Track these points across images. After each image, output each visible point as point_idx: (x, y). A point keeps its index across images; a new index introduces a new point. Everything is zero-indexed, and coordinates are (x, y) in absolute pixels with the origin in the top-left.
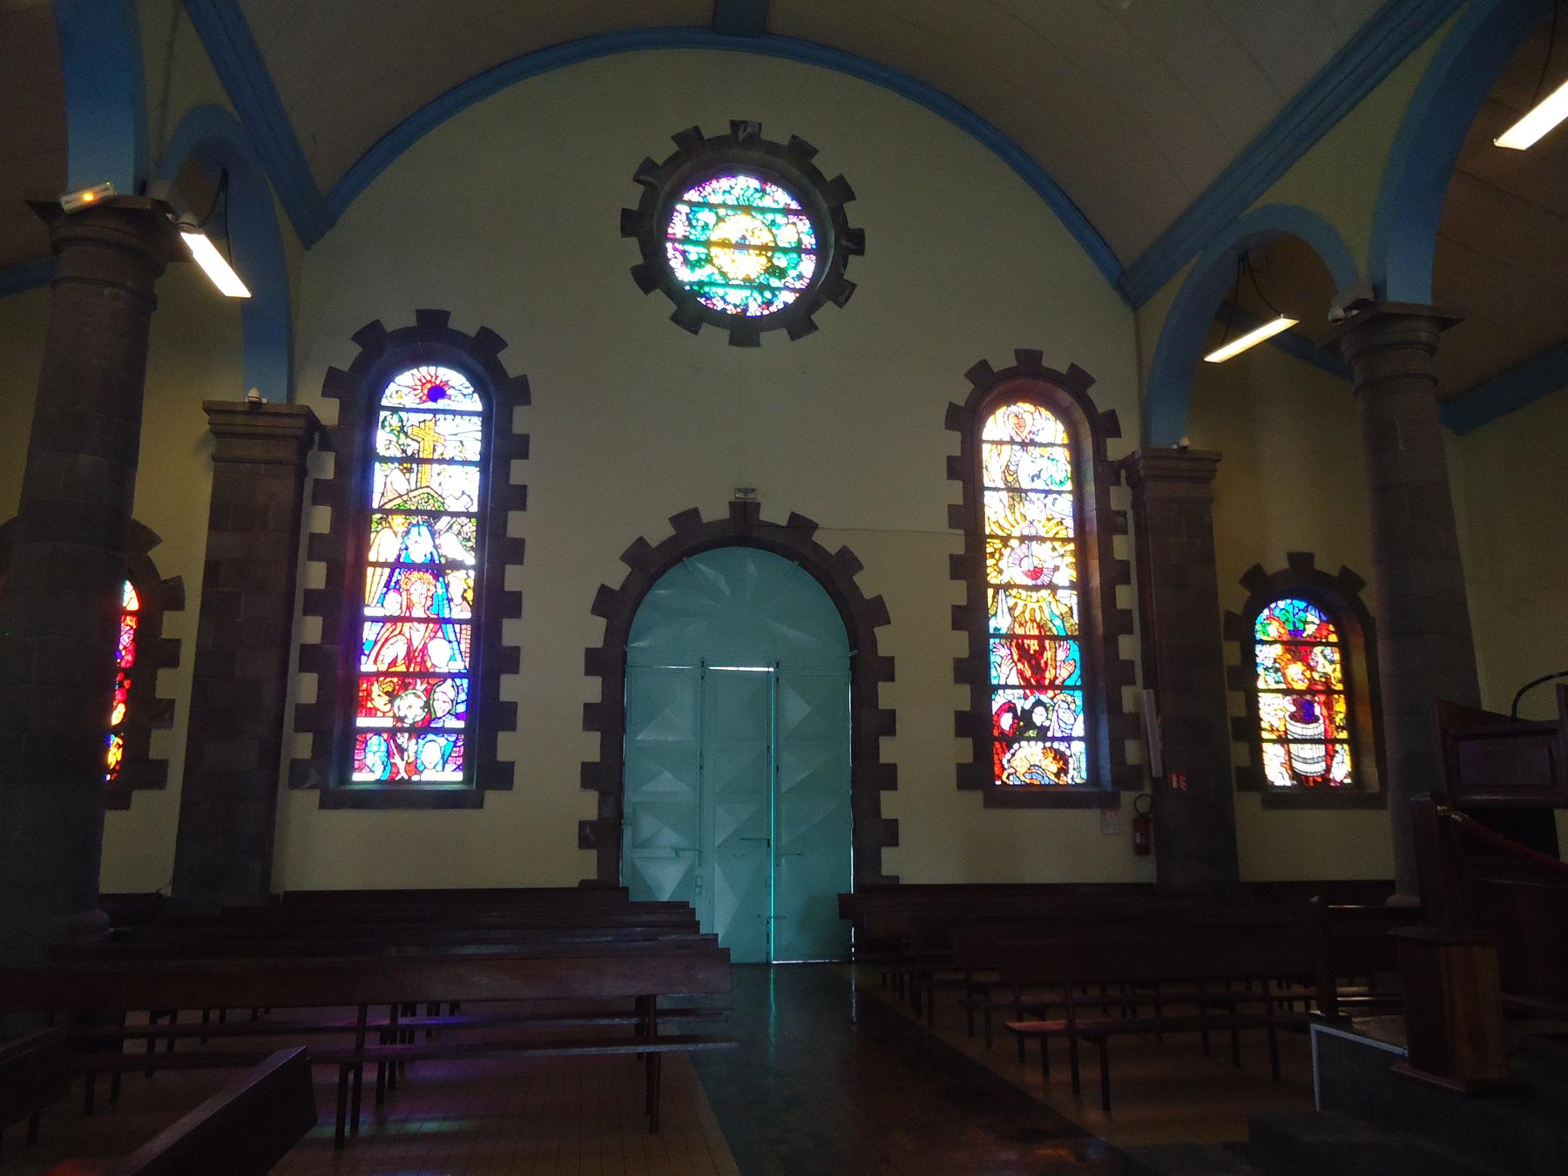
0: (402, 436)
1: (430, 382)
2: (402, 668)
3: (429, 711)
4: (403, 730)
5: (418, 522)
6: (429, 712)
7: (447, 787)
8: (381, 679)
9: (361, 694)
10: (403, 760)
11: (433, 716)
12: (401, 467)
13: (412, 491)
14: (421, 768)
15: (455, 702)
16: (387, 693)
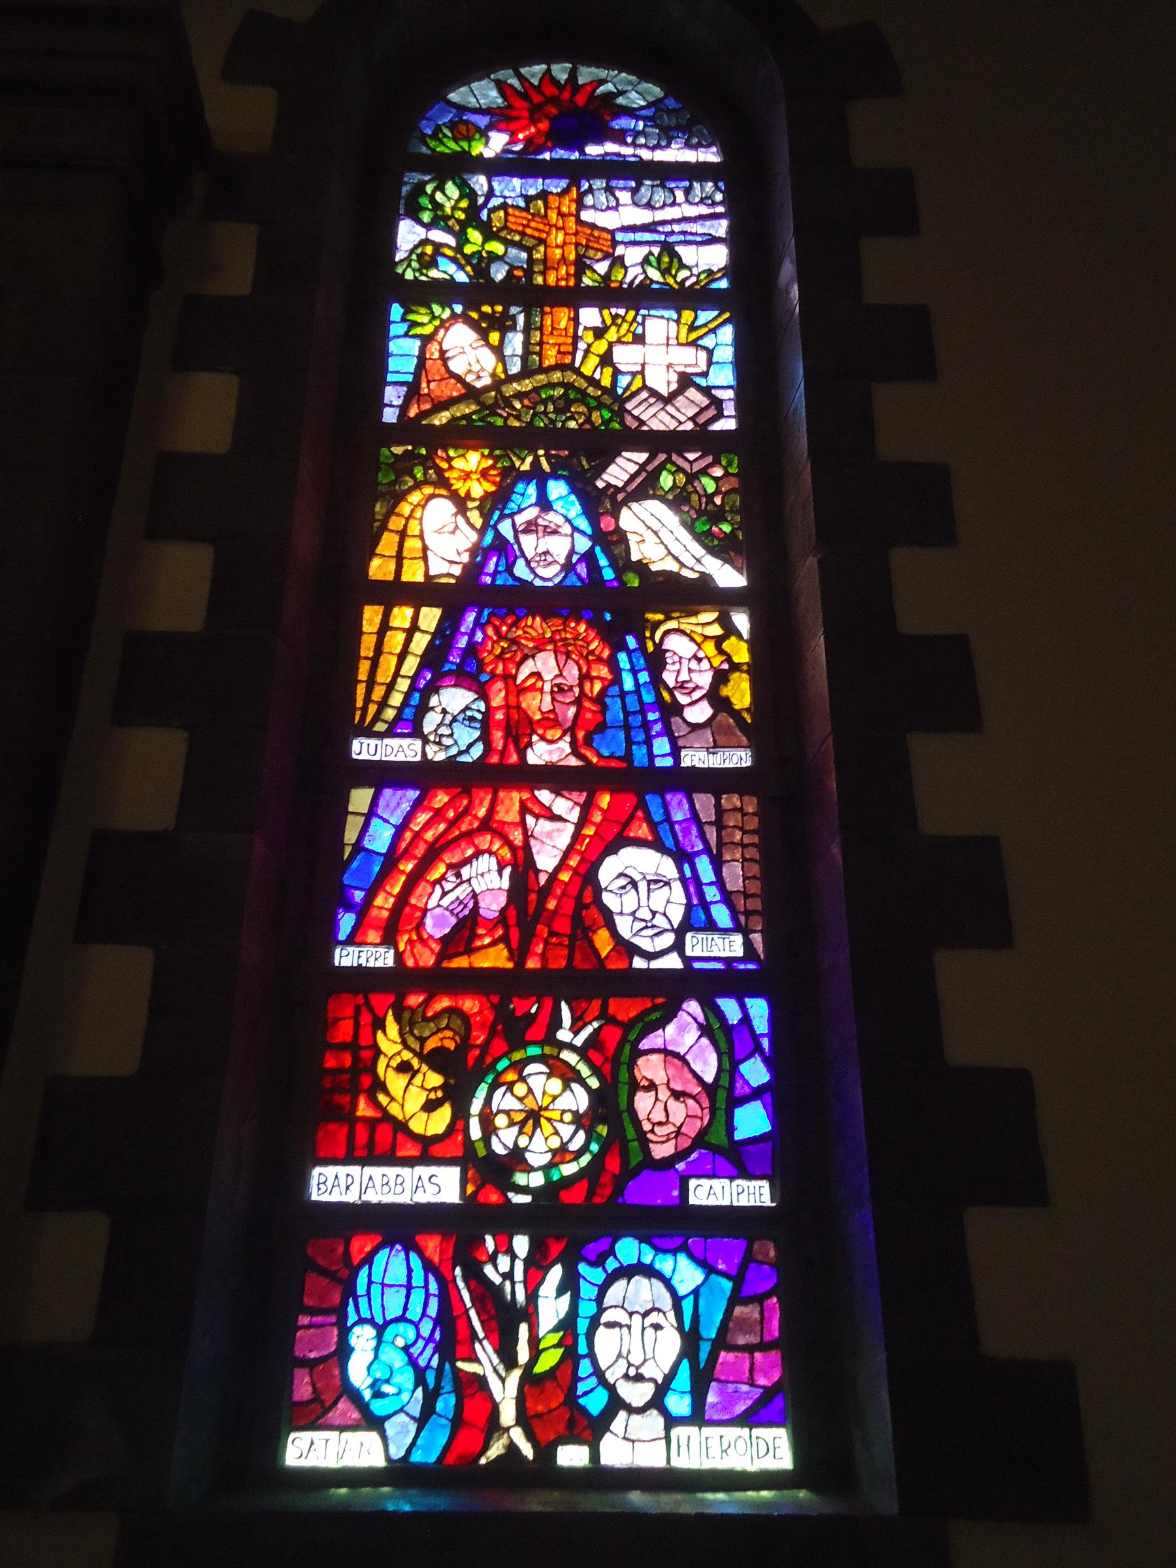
0: (474, 235)
1: (553, 100)
2: (495, 958)
3: (617, 1133)
4: (515, 1220)
5: (536, 463)
6: (615, 1143)
7: (718, 1500)
8: (415, 1000)
9: (330, 1063)
10: (509, 1361)
11: (636, 1158)
12: (474, 315)
13: (510, 379)
14: (595, 1403)
15: (722, 1095)
16: (436, 1060)
